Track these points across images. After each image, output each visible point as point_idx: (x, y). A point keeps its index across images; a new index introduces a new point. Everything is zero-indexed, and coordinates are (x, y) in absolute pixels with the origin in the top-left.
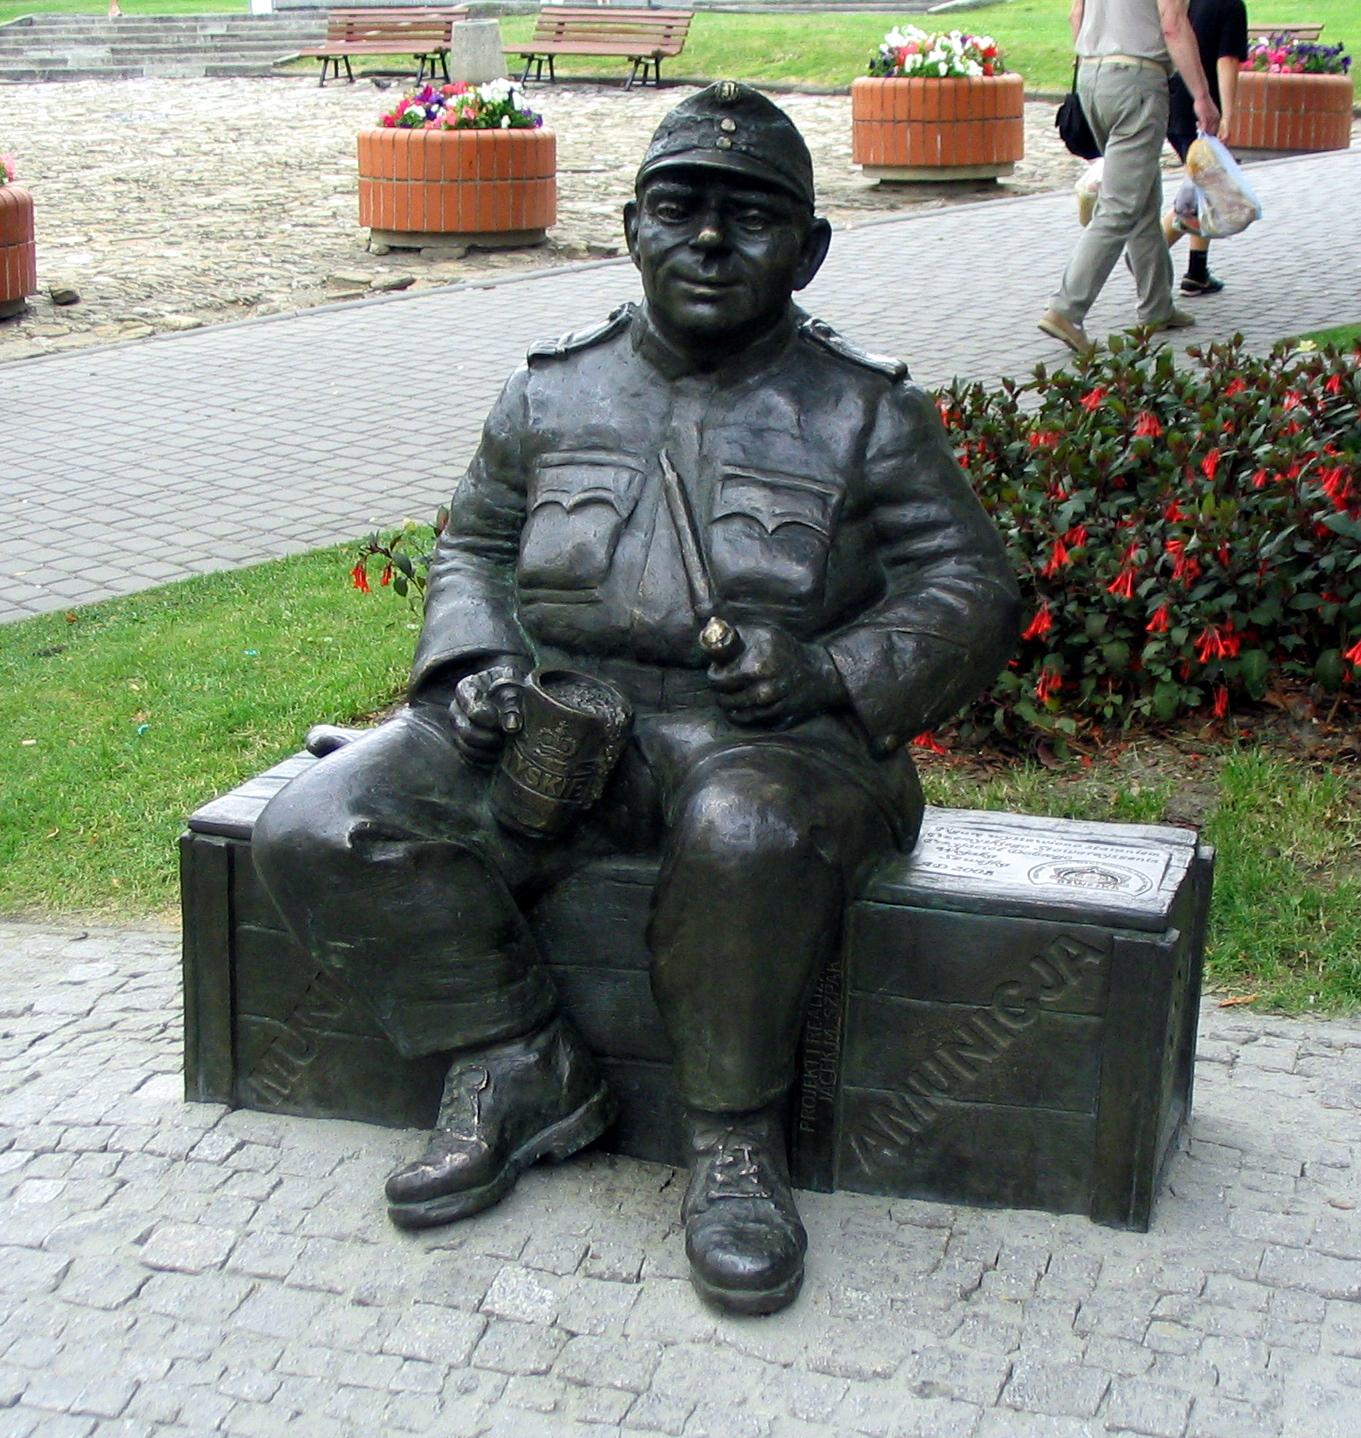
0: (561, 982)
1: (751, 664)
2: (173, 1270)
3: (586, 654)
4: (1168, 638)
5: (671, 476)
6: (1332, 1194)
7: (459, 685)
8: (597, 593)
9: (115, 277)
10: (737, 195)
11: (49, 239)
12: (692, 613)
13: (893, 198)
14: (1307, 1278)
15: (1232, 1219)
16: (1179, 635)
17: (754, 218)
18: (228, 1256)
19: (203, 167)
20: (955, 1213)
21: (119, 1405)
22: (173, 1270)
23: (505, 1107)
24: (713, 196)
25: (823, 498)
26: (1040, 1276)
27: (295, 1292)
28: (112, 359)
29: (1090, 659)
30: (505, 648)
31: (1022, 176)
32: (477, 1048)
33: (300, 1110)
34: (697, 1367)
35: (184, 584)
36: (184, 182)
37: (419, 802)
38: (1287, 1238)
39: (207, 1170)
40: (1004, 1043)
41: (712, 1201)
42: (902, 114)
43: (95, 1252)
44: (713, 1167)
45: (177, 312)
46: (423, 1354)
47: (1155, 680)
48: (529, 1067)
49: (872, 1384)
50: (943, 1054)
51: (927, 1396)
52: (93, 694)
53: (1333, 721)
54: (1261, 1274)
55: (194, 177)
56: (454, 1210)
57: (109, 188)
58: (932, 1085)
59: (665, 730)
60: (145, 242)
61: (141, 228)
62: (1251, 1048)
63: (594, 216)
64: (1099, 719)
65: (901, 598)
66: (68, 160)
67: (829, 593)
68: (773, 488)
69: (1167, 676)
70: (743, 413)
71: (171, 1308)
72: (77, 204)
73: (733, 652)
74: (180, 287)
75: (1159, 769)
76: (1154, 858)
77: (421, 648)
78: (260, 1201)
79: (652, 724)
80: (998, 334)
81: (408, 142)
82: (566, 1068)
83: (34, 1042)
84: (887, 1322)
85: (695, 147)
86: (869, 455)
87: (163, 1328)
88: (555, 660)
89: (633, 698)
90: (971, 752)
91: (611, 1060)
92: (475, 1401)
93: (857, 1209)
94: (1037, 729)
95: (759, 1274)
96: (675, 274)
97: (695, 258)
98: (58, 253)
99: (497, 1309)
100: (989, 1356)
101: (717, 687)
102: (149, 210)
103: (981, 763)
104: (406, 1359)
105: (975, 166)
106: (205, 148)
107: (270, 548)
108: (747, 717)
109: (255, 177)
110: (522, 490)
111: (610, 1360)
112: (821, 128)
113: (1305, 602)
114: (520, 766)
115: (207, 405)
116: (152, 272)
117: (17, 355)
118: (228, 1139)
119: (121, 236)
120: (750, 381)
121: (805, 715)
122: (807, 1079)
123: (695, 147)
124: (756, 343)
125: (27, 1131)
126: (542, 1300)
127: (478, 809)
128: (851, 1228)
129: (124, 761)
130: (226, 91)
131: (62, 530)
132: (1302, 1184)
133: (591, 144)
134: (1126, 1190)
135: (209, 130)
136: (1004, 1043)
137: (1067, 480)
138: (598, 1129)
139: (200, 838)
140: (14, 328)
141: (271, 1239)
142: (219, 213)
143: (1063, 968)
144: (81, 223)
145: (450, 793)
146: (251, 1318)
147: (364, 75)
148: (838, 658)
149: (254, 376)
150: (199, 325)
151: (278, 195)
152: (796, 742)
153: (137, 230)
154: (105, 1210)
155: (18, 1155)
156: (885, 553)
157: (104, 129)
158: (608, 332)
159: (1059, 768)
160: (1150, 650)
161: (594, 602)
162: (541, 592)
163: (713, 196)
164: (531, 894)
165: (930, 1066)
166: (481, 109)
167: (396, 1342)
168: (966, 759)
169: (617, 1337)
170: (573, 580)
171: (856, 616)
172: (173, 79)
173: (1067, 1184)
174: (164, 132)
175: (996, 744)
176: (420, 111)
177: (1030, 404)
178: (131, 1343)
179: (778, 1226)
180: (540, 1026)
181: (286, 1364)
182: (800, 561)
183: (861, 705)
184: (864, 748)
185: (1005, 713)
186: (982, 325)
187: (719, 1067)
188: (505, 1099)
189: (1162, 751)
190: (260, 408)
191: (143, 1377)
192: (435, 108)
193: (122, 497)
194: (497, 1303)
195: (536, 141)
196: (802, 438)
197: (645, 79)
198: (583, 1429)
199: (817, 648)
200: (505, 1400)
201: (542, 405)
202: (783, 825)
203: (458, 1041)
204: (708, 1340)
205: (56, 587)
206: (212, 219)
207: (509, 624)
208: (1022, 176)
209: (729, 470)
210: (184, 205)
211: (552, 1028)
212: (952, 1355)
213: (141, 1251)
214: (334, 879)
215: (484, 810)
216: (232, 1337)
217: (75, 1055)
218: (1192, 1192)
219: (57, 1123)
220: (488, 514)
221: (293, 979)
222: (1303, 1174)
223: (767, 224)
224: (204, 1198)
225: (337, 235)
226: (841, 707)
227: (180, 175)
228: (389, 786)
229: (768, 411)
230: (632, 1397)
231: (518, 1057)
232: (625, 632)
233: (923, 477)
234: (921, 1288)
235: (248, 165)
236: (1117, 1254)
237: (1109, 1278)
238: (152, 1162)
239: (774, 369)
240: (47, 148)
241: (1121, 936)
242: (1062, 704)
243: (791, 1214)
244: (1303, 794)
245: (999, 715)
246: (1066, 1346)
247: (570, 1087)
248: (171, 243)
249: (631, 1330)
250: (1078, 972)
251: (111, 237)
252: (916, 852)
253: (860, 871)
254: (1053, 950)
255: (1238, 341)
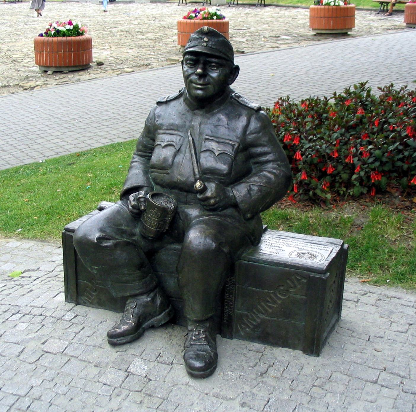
0: (159, 277)
1: (209, 194)
2: (50, 353)
3: (166, 188)
4: (359, 174)
5: (190, 139)
6: (376, 346)
7: (130, 196)
8: (169, 171)
9: (114, 58)
10: (208, 59)
11: (101, 47)
12: (193, 178)
13: (319, 38)
14: (362, 375)
15: (344, 354)
16: (362, 174)
17: (214, 66)
18: (65, 349)
19: (144, 27)
20: (265, 348)
21: (26, 393)
22: (50, 353)
23: (140, 313)
24: (202, 59)
25: (233, 146)
26: (284, 369)
27: (79, 362)
28: (108, 81)
29: (338, 178)
30: (146, 185)
31: (355, 32)
32: (135, 296)
33: (94, 306)
34: (182, 393)
35: (109, 146)
36: (138, 32)
37: (118, 228)
38: (359, 361)
39: (65, 323)
40: (280, 302)
41: (191, 345)
42: (322, 15)
43: (32, 345)
44: (192, 335)
45: (128, 68)
46: (109, 383)
47: (354, 185)
48: (147, 302)
49: (229, 402)
50: (263, 304)
51: (243, 407)
52: (79, 177)
53: (405, 197)
54: (348, 373)
55: (141, 30)
56: (124, 341)
57: (119, 33)
58: (260, 312)
59: (186, 210)
60: (125, 48)
61: (125, 44)
62: (364, 297)
63: (240, 42)
64: (339, 194)
65: (255, 174)
66: (111, 25)
67: (233, 173)
68: (218, 142)
69: (358, 184)
70: (213, 120)
71: (47, 365)
72: (110, 38)
73: (204, 190)
74: (130, 61)
75: (354, 210)
76: (328, 249)
77: (124, 184)
78: (77, 333)
79: (183, 208)
80: (338, 77)
81: (190, 23)
82: (159, 302)
83: (35, 280)
84: (237, 382)
85: (197, 46)
86: (247, 133)
87: (42, 371)
88: (157, 189)
89: (178, 201)
90: (303, 202)
91: (174, 299)
92: (120, 399)
93: (238, 345)
94: (321, 197)
95: (201, 367)
96: (191, 82)
97: (197, 77)
98: (102, 51)
99: (131, 371)
100: (264, 395)
101: (199, 199)
102: (127, 39)
103: (305, 206)
104: (104, 384)
105: (342, 29)
106: (146, 22)
107: (134, 135)
108: (208, 208)
109: (156, 31)
110: (154, 140)
111: (159, 389)
112: (305, 18)
113: (399, 164)
114: (145, 219)
115: (129, 94)
116: (123, 57)
117: (85, 79)
118: (73, 314)
119: (119, 47)
120: (215, 111)
121: (225, 207)
122: (226, 308)
123: (197, 46)
124: (217, 100)
125: (23, 308)
126: (144, 369)
127: (136, 230)
128: (235, 351)
129: (82, 196)
130: (154, 7)
131: (83, 129)
132: (368, 343)
133: (244, 22)
134: (313, 346)
135: (148, 17)
136: (280, 302)
137: (337, 126)
138: (168, 319)
139: (67, 233)
140: (86, 72)
141: (77, 345)
142: (145, 40)
143: (296, 283)
144: (109, 43)
145: (128, 226)
146: (66, 369)
147: (190, 3)
148: (234, 192)
149: (142, 86)
150: (133, 71)
151: (160, 36)
152: (220, 216)
153: (123, 45)
154: (37, 333)
155: (20, 315)
156: (252, 161)
157: (122, 17)
158: (179, 95)
159: (327, 208)
160: (354, 177)
161: (168, 174)
162: (155, 170)
163: (202, 59)
164: (151, 254)
165: (259, 307)
166: (209, 14)
167: (103, 379)
168: (301, 204)
169: (162, 381)
170: (164, 167)
171: (242, 179)
172: (142, 3)
173: (297, 342)
174: (137, 18)
175: (310, 200)
176: (193, 15)
177: (332, 102)
178: (34, 374)
179: (209, 353)
180: (151, 291)
181: (73, 384)
182: (224, 164)
183: (242, 206)
184: (242, 217)
185: (313, 192)
186: (334, 75)
187: (193, 308)
188: (141, 311)
189: (355, 204)
190: (142, 95)
191: (34, 385)
192: (197, 14)
193: (101, 120)
194: (132, 369)
195: (224, 23)
196: (228, 128)
197: (261, 4)
198: (147, 410)
199: (229, 189)
200: (128, 399)
201: (159, 116)
202: (211, 242)
203: (128, 294)
204: (186, 385)
205: (78, 145)
206: (142, 42)
207: (148, 178)
208: (355, 32)
209: (207, 137)
210: (136, 38)
211: (156, 290)
212: (253, 394)
213: (43, 346)
214: (92, 250)
215: (137, 230)
216: (60, 375)
217: (43, 285)
218: (335, 344)
219: (32, 306)
220: (145, 146)
221: (88, 273)
222: (369, 340)
223: (218, 68)
224: (63, 331)
225: (173, 47)
226: (235, 206)
227: (138, 30)
228: (113, 222)
229: (219, 120)
230: (162, 400)
231: (146, 299)
232: (176, 183)
233: (263, 139)
234: (249, 372)
235: (155, 27)
236: (308, 364)
237: (305, 371)
238: (52, 320)
239: (222, 108)
240: (106, 22)
241: (312, 275)
242: (330, 189)
243: (214, 348)
244: (392, 219)
245: (311, 193)
246: (286, 393)
247: (160, 308)
248: (131, 49)
249: (166, 380)
250: (300, 284)
251: (116, 47)
252: (259, 245)
253: (239, 252)
254: (293, 277)
255: (392, 85)
